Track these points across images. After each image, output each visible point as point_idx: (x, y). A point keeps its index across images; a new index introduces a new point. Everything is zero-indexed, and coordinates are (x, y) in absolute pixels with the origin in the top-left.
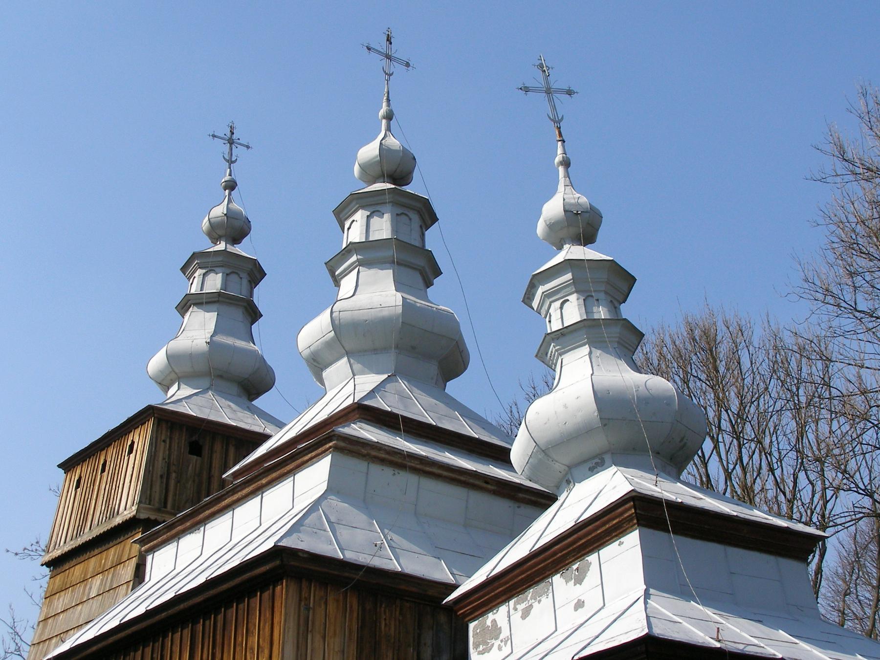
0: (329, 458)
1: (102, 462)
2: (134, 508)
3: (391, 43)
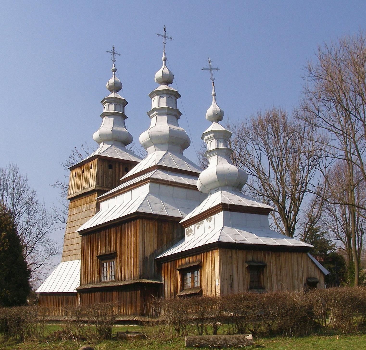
0: (149, 184)
1: (82, 169)
2: (94, 186)
3: (165, 32)
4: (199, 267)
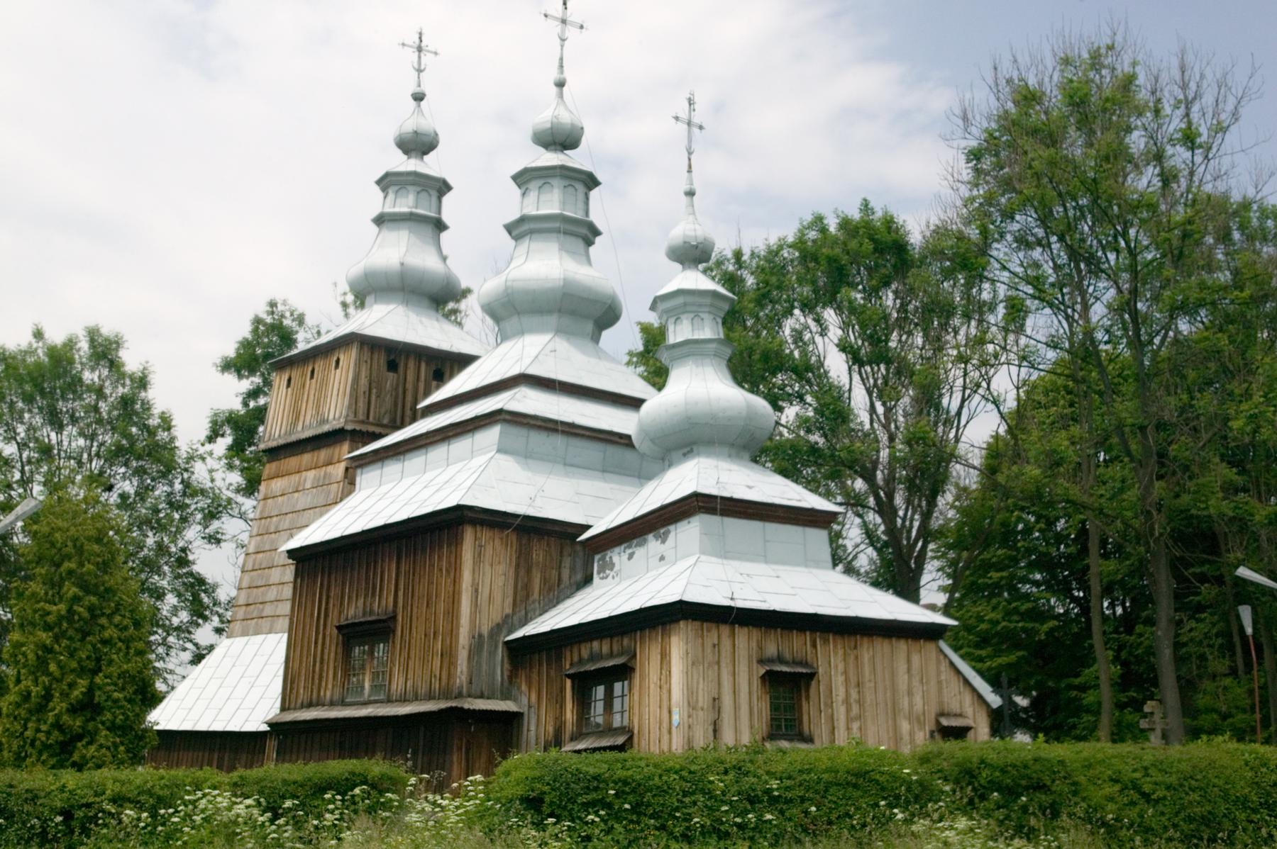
2: (342, 420)
4: (624, 672)
